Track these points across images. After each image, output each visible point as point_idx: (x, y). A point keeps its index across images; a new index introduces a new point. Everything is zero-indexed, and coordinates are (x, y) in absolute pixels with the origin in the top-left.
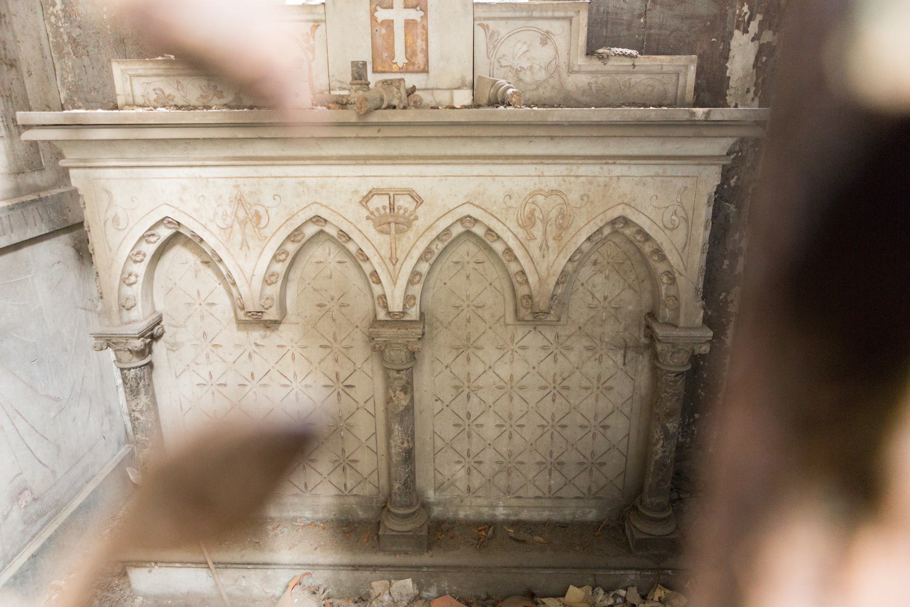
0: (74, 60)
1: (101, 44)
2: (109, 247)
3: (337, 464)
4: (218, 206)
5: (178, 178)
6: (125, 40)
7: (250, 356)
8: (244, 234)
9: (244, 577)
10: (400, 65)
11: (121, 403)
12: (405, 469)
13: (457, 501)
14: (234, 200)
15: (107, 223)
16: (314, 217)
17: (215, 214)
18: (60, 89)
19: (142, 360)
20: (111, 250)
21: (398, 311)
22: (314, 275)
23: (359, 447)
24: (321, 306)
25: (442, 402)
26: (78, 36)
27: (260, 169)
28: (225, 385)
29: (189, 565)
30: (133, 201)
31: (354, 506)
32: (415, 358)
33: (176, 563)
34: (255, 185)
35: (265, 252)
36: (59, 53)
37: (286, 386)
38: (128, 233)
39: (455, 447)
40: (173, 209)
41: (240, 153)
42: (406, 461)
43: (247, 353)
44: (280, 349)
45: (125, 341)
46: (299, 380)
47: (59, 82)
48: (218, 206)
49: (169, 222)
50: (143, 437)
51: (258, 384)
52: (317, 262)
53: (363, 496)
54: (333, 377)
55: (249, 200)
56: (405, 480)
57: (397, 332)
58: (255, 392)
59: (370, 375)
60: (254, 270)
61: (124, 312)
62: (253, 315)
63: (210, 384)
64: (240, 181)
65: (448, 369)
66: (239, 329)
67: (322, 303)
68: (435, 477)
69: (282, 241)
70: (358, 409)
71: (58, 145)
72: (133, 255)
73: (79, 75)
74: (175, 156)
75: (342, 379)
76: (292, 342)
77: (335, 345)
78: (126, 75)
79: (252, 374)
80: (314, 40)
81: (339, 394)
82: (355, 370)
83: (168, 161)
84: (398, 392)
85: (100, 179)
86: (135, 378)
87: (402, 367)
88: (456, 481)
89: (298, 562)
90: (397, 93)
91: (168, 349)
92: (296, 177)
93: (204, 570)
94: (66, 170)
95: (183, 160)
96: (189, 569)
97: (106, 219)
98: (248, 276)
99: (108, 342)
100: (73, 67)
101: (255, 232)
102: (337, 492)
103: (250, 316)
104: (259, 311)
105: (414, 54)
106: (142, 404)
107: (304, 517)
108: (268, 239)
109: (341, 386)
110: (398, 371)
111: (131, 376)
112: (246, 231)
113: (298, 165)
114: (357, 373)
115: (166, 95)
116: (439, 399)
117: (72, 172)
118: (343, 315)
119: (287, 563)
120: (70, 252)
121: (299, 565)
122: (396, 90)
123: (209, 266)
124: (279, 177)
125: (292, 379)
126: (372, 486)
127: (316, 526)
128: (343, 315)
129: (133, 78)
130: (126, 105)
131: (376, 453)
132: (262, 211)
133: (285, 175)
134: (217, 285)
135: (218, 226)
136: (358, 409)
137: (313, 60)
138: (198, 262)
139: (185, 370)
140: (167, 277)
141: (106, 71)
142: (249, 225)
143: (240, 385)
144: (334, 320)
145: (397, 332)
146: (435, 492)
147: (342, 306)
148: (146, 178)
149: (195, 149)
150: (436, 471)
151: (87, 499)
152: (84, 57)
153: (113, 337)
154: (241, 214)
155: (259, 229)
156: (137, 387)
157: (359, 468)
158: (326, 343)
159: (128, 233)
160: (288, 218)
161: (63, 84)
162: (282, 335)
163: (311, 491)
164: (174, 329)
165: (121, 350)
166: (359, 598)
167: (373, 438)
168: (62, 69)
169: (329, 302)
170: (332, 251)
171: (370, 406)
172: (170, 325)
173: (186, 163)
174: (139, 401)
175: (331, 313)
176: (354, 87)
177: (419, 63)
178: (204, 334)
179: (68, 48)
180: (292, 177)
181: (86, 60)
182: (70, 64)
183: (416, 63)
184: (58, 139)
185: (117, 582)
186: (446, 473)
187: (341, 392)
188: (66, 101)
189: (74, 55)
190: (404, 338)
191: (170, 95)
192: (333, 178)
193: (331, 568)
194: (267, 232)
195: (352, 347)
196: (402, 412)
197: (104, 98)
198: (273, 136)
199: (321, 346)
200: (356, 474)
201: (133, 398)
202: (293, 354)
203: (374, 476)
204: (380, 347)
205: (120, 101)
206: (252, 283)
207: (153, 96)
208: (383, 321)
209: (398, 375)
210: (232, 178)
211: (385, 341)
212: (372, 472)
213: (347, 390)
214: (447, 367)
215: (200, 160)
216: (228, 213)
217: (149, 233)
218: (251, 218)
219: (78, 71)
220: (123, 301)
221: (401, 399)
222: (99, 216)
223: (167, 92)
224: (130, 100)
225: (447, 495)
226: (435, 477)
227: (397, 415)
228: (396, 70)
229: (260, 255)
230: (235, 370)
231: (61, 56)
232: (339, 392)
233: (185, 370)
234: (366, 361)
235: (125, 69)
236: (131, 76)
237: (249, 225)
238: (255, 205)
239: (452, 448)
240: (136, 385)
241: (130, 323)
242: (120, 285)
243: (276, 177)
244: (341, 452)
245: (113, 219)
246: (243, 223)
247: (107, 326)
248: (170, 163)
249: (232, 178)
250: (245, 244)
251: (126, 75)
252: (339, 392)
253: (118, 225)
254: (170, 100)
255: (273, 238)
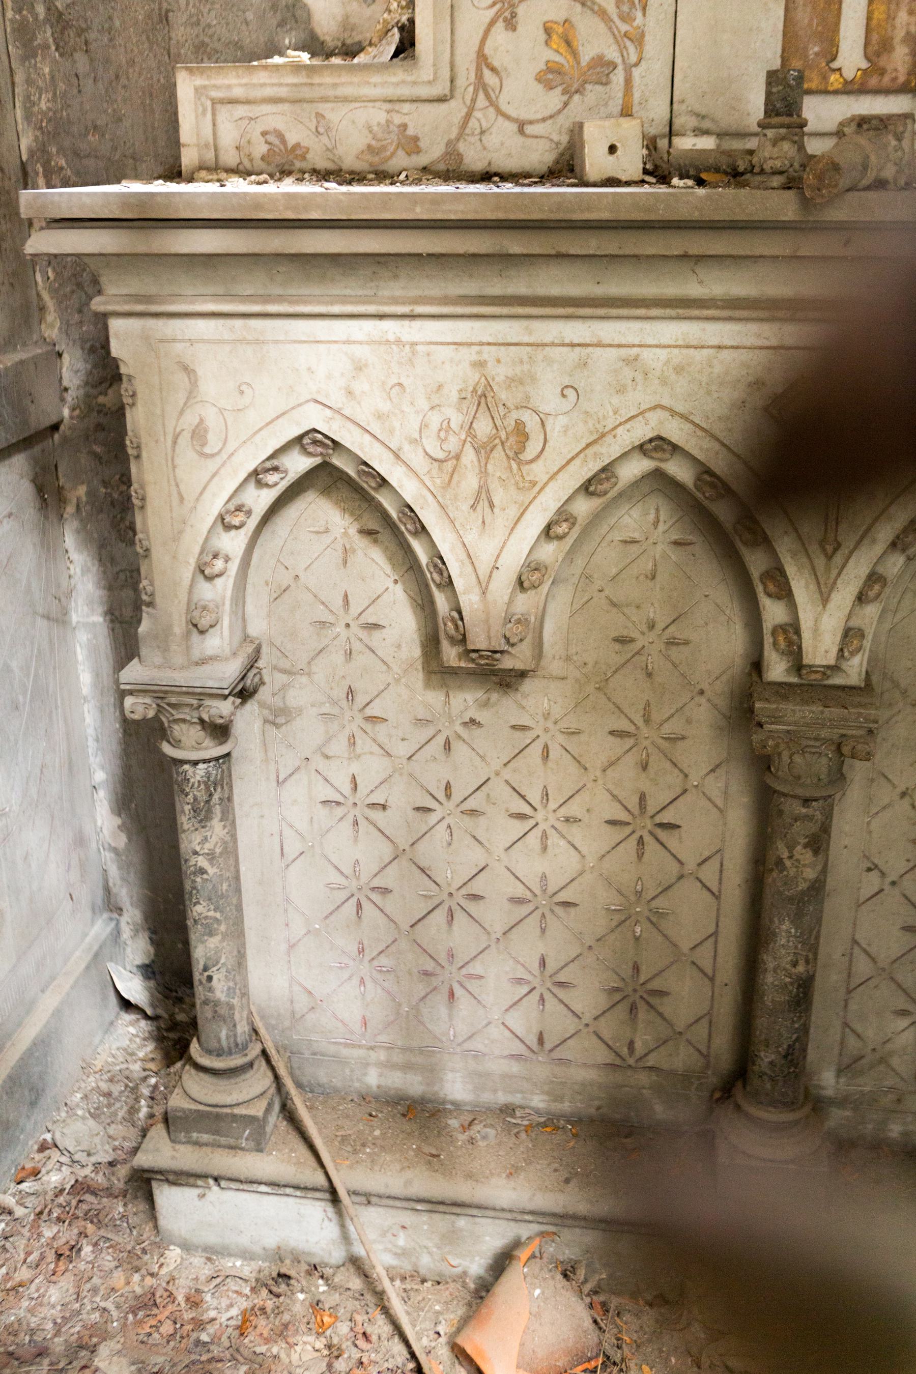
0: (57, 61)
1: (117, 23)
2: (180, 493)
3: (618, 997)
4: (432, 408)
5: (348, 342)
6: (170, 14)
7: (447, 746)
8: (484, 473)
9: (404, 1227)
10: (849, 74)
11: (99, 823)
12: (793, 1022)
13: (887, 1100)
14: (469, 396)
15: (179, 441)
16: (651, 441)
17: (424, 426)
18: (20, 127)
19: (221, 744)
20: (182, 499)
21: (824, 663)
22: (614, 571)
23: (672, 963)
24: (622, 641)
25: (883, 874)
26: (68, 6)
27: (536, 324)
28: (384, 807)
29: (288, 1191)
30: (242, 392)
31: (644, 1091)
32: (842, 774)
33: (260, 1183)
34: (521, 362)
35: (528, 515)
36: (25, 46)
37: (522, 817)
38: (223, 465)
39: (900, 978)
40: (328, 412)
41: (496, 288)
42: (798, 1003)
43: (440, 740)
44: (518, 734)
45: (195, 702)
46: (552, 805)
47: (19, 112)
48: (432, 408)
49: (315, 442)
50: (209, 910)
51: (460, 809)
52: (625, 542)
53: (672, 1073)
54: (633, 802)
55: (503, 395)
56: (789, 1046)
57: (822, 713)
58: (449, 827)
59: (719, 802)
60: (498, 557)
61: (195, 636)
62: (481, 657)
63: (351, 801)
64: (489, 353)
65: (907, 799)
66: (428, 684)
67: (625, 634)
68: (842, 1043)
69: (571, 491)
70: (681, 877)
71: (91, 263)
72: (227, 512)
73: (64, 94)
74: (348, 292)
75: (651, 810)
76: (546, 719)
77: (645, 731)
78: (203, 99)
79: (448, 787)
80: (644, 15)
81: (641, 841)
82: (685, 791)
83: (332, 304)
84: (799, 848)
85: (174, 340)
86: (206, 783)
87: (817, 794)
88: (891, 1054)
89: (530, 1206)
90: (896, 151)
91: (266, 721)
92: (619, 346)
93: (318, 1203)
94: (102, 318)
95: (364, 303)
96: (285, 1199)
97: (178, 430)
98: (483, 571)
99: (159, 701)
100: (53, 78)
101: (511, 468)
102: (610, 1058)
103: (473, 660)
104: (497, 649)
105: (886, 46)
106: (214, 839)
107: (529, 1107)
108: (537, 488)
109: (649, 824)
110: (806, 801)
111: (198, 778)
112: (490, 467)
113: (628, 318)
114: (688, 797)
115: (289, 147)
116: (876, 866)
117: (115, 325)
118: (673, 664)
119: (505, 1207)
120: (26, 489)
121: (532, 1213)
122: (894, 143)
123: (375, 541)
124: (579, 345)
125: (536, 802)
126: (692, 1050)
127: (557, 1128)
128: (673, 664)
129: (218, 106)
130: (201, 168)
131: (712, 979)
132: (531, 422)
133: (595, 341)
134: (391, 585)
135: (427, 454)
136: (681, 877)
137: (636, 65)
138: (353, 531)
139: (298, 768)
140: (278, 561)
141: (124, 87)
142: (498, 453)
143: (418, 809)
144: (649, 675)
145: (822, 713)
146: (838, 1076)
147: (672, 643)
148: (276, 342)
149: (396, 277)
150: (847, 1030)
151: (45, 1026)
152: (77, 55)
153: (173, 692)
154: (483, 427)
155: (520, 463)
156: (207, 802)
157: (667, 1010)
158: (624, 725)
159: (223, 465)
160: (589, 441)
161: (28, 117)
162: (524, 703)
163: (551, 1051)
164: (284, 678)
165: (184, 721)
166: (656, 1297)
167: (710, 943)
168: (29, 82)
169: (643, 633)
170: (662, 519)
171: (709, 874)
172: (275, 668)
173: (371, 309)
174: (209, 834)
175: (644, 658)
176: (770, 133)
177: (896, 70)
178: (350, 691)
179: (47, 35)
180: (611, 346)
181: (82, 62)
182: (47, 70)
183: (889, 68)
184: (104, 252)
185: (121, 1209)
186: (870, 1033)
187: (648, 838)
188: (31, 153)
189: (57, 49)
190: (837, 727)
191: (297, 146)
192: (705, 352)
193: (603, 1226)
194: (539, 471)
195: (683, 738)
196: (803, 893)
197: (114, 148)
198: (591, 252)
199: (612, 733)
200: (659, 1020)
201: (197, 825)
202: (546, 747)
203: (702, 1030)
204: (777, 745)
205: (188, 158)
206: (491, 587)
207: (260, 149)
208: (780, 684)
209: (804, 811)
210: (472, 344)
211: (788, 732)
212: (697, 1021)
213: (662, 834)
214: (903, 795)
215: (404, 303)
216: (453, 425)
217: (268, 465)
218: (503, 437)
219: (62, 86)
220: (196, 614)
221: (804, 865)
222: (164, 425)
223: (292, 140)
224: (210, 156)
225: (866, 1084)
226: (842, 1043)
227: (791, 899)
228: (837, 86)
229: (516, 524)
230: (411, 775)
231: (29, 53)
232: (641, 837)
233: (298, 768)
234: (713, 771)
235: (205, 87)
236: (214, 102)
237: (498, 453)
238: (517, 408)
239: (892, 979)
240: (205, 798)
241: (202, 662)
242: (193, 580)
243: (573, 345)
244: (630, 972)
245: (194, 431)
246: (484, 450)
247: (159, 667)
248: (336, 309)
249: (472, 344)
250: (483, 496)
251: (203, 99)
252: (641, 837)
253: (203, 445)
254: (296, 157)
255: (551, 484)
